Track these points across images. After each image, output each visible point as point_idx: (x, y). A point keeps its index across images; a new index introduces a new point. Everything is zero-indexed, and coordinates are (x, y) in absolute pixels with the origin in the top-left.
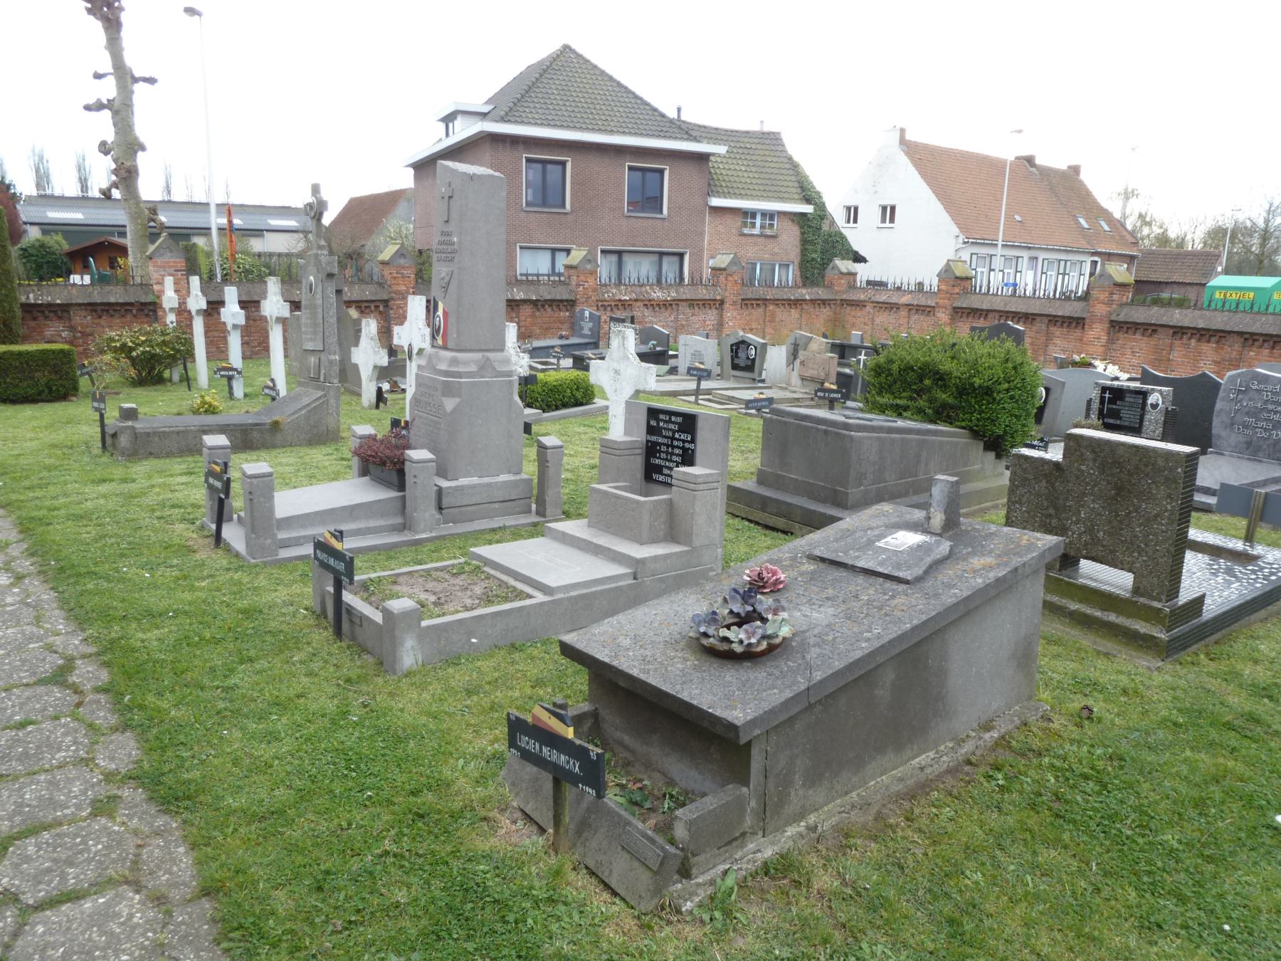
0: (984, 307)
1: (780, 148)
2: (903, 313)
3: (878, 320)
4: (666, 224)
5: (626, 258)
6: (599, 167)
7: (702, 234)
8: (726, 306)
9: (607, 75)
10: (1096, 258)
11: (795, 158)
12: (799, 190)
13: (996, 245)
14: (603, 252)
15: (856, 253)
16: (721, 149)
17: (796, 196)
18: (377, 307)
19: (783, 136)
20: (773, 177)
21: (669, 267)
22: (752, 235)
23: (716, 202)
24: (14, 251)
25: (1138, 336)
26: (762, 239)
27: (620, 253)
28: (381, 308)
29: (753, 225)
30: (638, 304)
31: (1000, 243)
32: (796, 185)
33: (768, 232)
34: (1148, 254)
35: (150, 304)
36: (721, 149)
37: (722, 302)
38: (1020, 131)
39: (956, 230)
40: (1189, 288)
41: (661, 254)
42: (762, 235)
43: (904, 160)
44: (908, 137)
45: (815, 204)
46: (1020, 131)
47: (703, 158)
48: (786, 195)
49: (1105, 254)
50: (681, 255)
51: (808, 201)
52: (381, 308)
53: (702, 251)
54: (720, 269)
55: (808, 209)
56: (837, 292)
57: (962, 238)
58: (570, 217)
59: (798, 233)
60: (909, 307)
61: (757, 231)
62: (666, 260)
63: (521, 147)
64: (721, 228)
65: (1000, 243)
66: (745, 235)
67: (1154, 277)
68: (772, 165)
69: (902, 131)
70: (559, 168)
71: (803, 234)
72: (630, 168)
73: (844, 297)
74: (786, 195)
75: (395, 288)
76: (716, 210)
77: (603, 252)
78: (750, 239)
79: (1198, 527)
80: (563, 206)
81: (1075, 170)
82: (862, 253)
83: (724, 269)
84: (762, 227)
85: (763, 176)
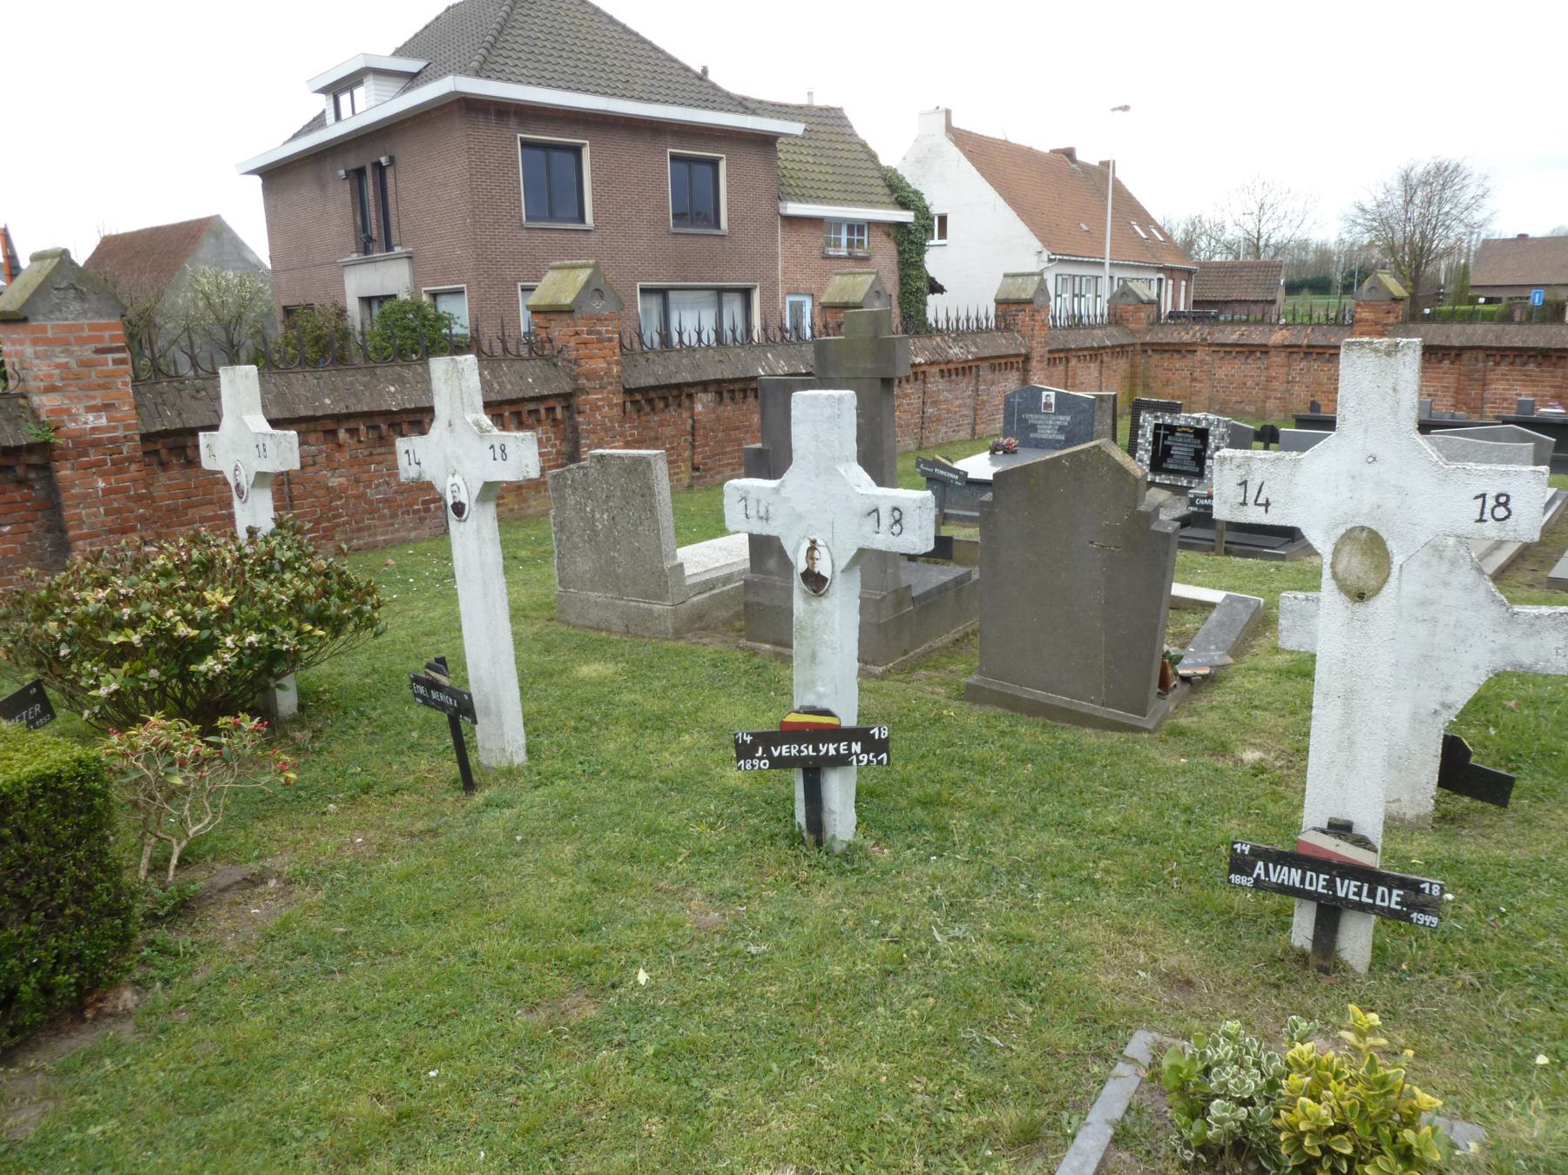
0: (1456, 343)
1: (847, 131)
2: (1277, 359)
3: (1220, 373)
4: (727, 243)
5: (672, 295)
6: (628, 151)
7: (774, 257)
8: (1034, 363)
9: (605, 14)
10: (1161, 275)
11: (872, 145)
12: (887, 191)
13: (1102, 264)
14: (643, 290)
15: (932, 279)
16: (797, 128)
17: (885, 199)
18: (551, 410)
19: (847, 112)
20: (851, 172)
21: (733, 308)
22: (839, 258)
23: (793, 208)
24: (524, 302)
25: (1504, 368)
26: (850, 263)
27: (663, 292)
28: (559, 413)
29: (838, 245)
30: (935, 369)
31: (1107, 262)
32: (881, 183)
33: (860, 253)
34: (1207, 267)
35: (30, 448)
36: (797, 128)
37: (1027, 358)
38: (1126, 108)
39: (1037, 245)
40: (1253, 307)
41: (720, 291)
42: (850, 257)
43: (954, 153)
44: (955, 124)
45: (916, 210)
46: (1126, 108)
47: (766, 141)
48: (871, 197)
49: (1172, 269)
50: (746, 293)
51: (904, 205)
52: (559, 413)
53: (775, 283)
54: (1019, 302)
55: (907, 216)
56: (1133, 333)
57: (1046, 254)
58: (593, 238)
59: (895, 253)
60: (1290, 349)
61: (844, 252)
62: (726, 297)
63: (513, 122)
64: (798, 248)
65: (1107, 262)
66: (829, 257)
67: (1210, 296)
68: (848, 155)
69: (948, 113)
70: (570, 157)
71: (900, 253)
72: (674, 158)
73: (1148, 339)
74: (871, 197)
75: (589, 365)
76: (791, 220)
77: (643, 290)
78: (836, 263)
79: (1185, 582)
80: (582, 219)
81: (1105, 164)
82: (940, 281)
83: (1030, 302)
84: (850, 244)
85: (838, 170)
